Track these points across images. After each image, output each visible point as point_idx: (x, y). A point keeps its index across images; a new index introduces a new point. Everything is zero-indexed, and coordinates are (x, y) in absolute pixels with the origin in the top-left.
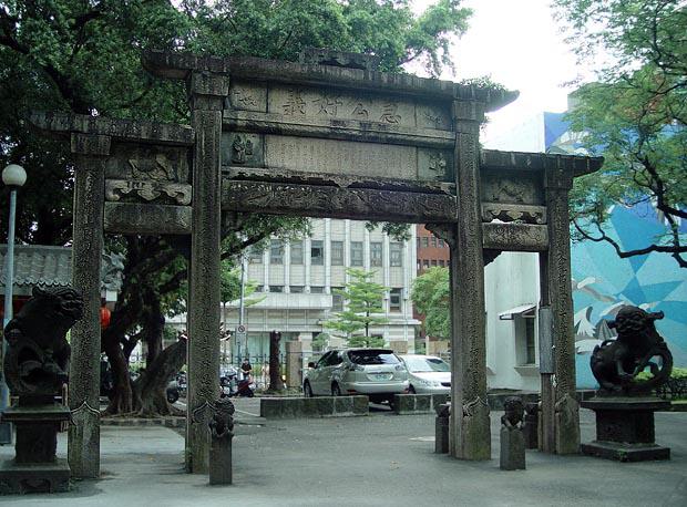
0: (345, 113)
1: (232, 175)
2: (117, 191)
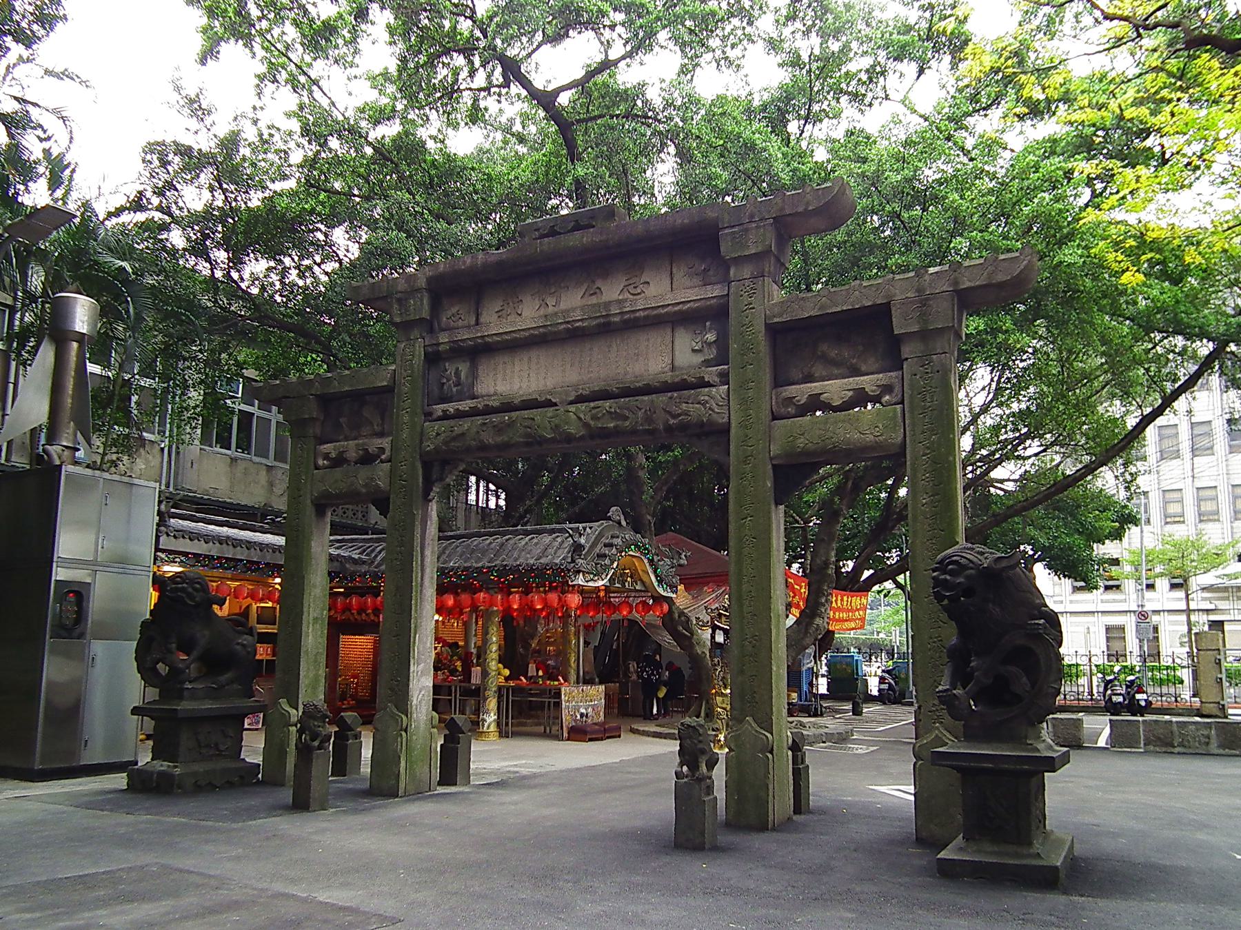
0: (572, 303)
1: (435, 416)
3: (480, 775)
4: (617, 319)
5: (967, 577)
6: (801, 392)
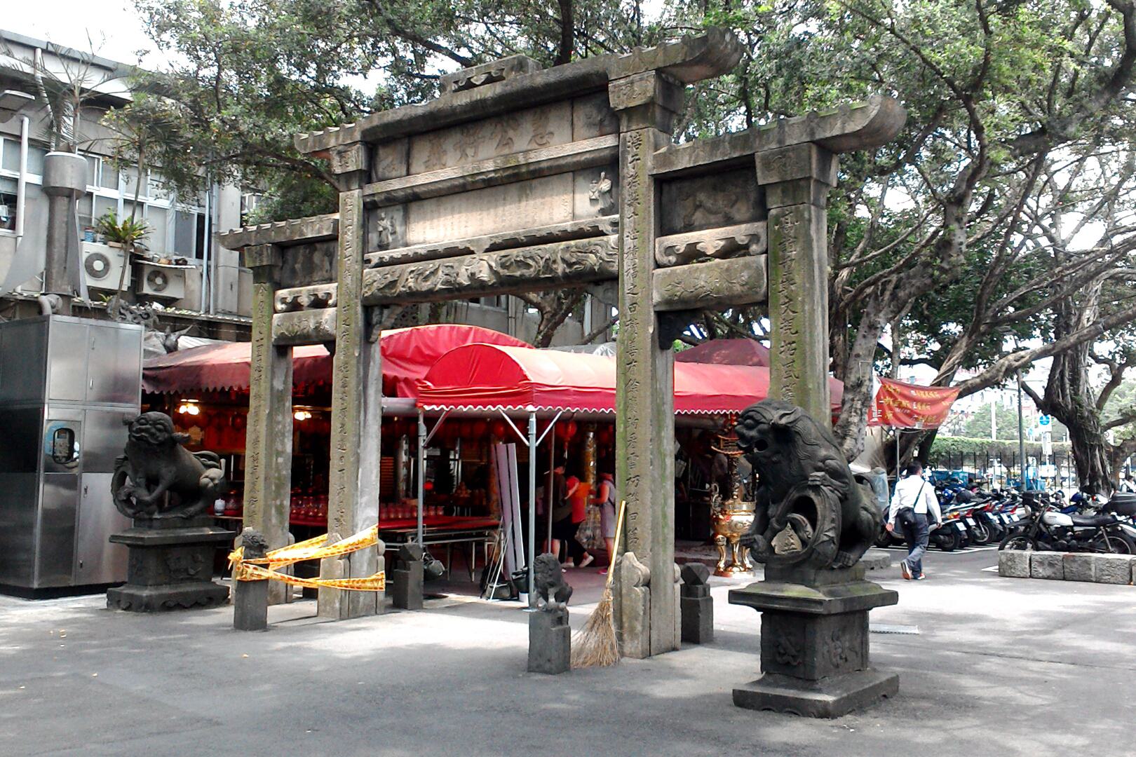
0: (486, 157)
1: (373, 263)
2: (283, 301)
3: (522, 621)
4: (524, 170)
5: (759, 431)
6: (680, 241)
